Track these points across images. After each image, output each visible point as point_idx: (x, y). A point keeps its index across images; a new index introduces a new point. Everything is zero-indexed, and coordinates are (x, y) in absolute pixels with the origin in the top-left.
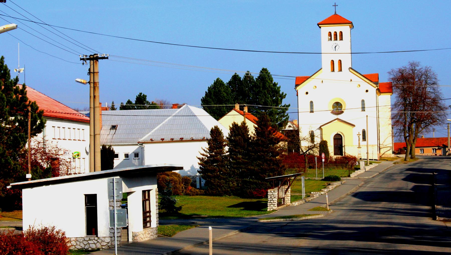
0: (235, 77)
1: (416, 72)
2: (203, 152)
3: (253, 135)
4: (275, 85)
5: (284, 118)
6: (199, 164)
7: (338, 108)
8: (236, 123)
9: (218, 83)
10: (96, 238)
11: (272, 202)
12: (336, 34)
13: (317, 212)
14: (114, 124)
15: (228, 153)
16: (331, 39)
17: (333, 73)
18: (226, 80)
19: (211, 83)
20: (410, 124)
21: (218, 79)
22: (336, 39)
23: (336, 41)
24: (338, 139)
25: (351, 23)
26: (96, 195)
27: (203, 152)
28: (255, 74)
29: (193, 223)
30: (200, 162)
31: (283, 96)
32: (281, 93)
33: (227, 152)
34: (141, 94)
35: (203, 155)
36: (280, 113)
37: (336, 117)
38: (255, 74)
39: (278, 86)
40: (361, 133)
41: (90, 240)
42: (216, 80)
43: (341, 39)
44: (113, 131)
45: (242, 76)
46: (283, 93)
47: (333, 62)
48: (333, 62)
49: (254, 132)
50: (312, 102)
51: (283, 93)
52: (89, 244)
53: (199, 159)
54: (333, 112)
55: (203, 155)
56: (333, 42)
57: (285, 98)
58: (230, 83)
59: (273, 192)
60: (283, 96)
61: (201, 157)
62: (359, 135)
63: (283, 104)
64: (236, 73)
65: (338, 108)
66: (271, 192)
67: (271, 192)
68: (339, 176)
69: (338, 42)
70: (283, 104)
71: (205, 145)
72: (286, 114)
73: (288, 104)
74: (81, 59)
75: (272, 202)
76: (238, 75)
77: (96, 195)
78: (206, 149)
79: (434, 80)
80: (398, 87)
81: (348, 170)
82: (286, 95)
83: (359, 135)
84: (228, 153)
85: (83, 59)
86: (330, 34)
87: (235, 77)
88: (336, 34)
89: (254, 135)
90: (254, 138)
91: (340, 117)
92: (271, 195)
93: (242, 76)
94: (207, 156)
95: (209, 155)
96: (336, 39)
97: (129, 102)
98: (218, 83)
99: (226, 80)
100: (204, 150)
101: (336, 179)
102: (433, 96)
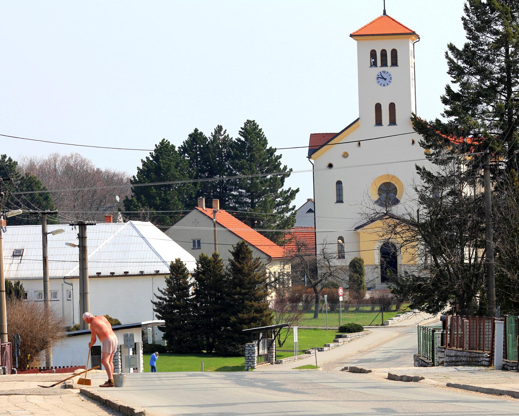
0: (196, 137)
2: (160, 295)
5: (290, 213)
6: (155, 310)
8: (205, 255)
9: (164, 149)
11: (250, 358)
12: (384, 53)
14: (18, 247)
15: (194, 296)
17: (379, 127)
18: (178, 141)
21: (162, 143)
22: (384, 64)
23: (384, 69)
25: (413, 33)
27: (160, 295)
28: (234, 133)
30: (155, 308)
31: (286, 173)
32: (282, 167)
34: (4, 157)
35: (161, 298)
36: (279, 204)
38: (234, 133)
42: (158, 144)
43: (395, 63)
44: (17, 260)
45: (208, 133)
46: (285, 168)
47: (378, 107)
48: (378, 107)
50: (339, 183)
51: (285, 168)
55: (161, 298)
56: (379, 69)
57: (288, 175)
58: (185, 149)
59: (251, 346)
60: (286, 173)
61: (157, 300)
63: (285, 188)
64: (196, 130)
66: (249, 346)
67: (249, 346)
68: (361, 324)
69: (390, 69)
70: (285, 188)
71: (164, 286)
72: (291, 206)
73: (294, 189)
75: (250, 358)
76: (201, 133)
78: (163, 291)
81: (381, 313)
82: (291, 170)
84: (194, 296)
86: (373, 54)
87: (196, 137)
88: (384, 53)
92: (249, 350)
94: (165, 299)
95: (168, 299)
98: (164, 149)
99: (178, 141)
100: (161, 291)
101: (357, 329)
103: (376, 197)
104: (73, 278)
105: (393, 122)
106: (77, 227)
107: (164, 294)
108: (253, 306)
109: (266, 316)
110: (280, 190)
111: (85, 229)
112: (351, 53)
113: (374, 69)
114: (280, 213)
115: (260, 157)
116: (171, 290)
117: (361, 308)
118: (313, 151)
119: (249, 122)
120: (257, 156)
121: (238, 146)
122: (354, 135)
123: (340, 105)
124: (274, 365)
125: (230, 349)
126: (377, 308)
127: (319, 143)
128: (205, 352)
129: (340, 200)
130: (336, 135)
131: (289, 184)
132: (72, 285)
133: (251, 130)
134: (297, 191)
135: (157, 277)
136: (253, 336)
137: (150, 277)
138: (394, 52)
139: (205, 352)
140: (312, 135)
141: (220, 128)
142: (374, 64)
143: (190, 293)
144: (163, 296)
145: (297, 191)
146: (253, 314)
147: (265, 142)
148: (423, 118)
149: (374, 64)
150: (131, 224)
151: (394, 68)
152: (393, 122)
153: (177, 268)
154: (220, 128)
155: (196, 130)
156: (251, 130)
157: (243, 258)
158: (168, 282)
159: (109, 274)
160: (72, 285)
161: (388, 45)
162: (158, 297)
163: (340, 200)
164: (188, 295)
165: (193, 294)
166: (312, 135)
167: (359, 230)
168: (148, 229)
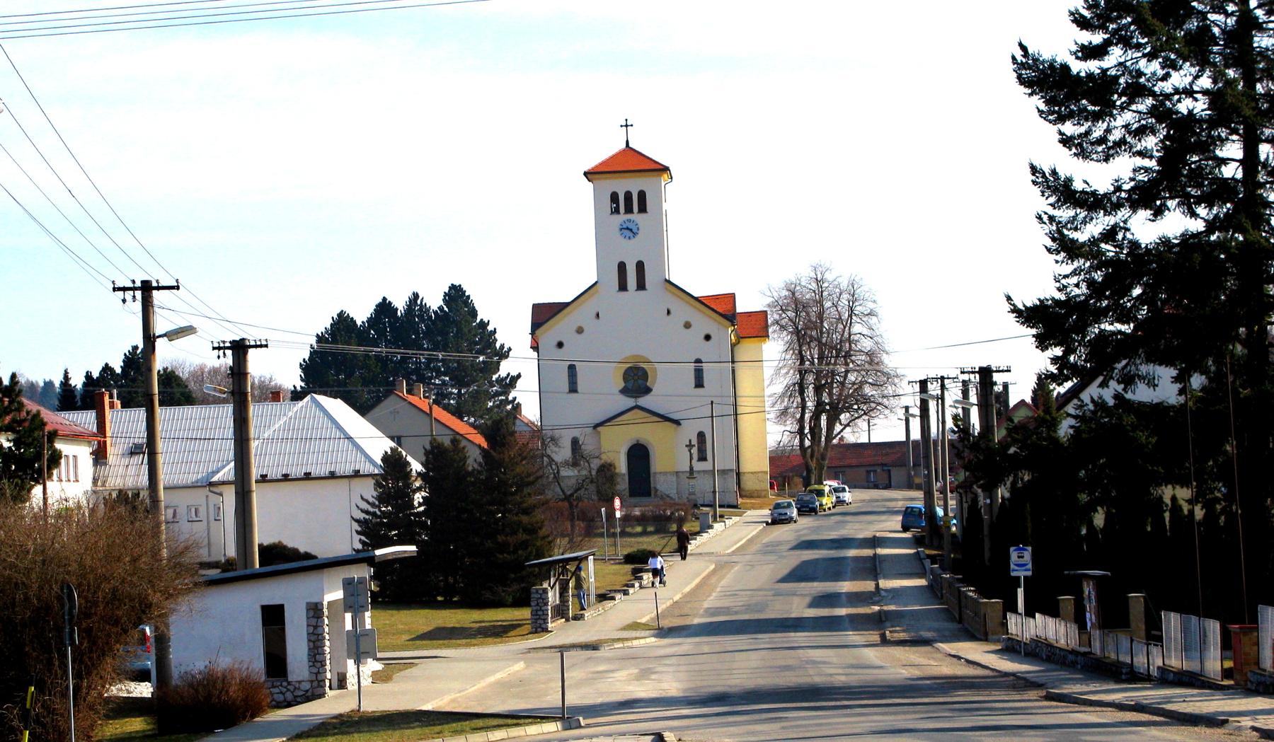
0: (384, 308)
1: (826, 285)
2: (365, 506)
3: (476, 466)
4: (484, 325)
6: (358, 533)
7: (637, 381)
9: (343, 324)
10: (285, 684)
12: (628, 196)
13: (638, 634)
16: (617, 211)
18: (361, 314)
19: (323, 323)
20: (816, 417)
21: (341, 314)
22: (629, 210)
23: (629, 216)
24: (639, 455)
26: (282, 607)
27: (365, 506)
28: (434, 300)
29: (713, 615)
31: (504, 354)
32: (498, 345)
33: (420, 505)
35: (367, 512)
36: (497, 394)
37: (630, 402)
38: (434, 300)
39: (490, 328)
40: (694, 442)
41: (273, 687)
43: (643, 209)
47: (622, 267)
48: (622, 267)
49: (480, 459)
51: (502, 346)
52: (272, 694)
53: (357, 521)
54: (624, 391)
55: (367, 512)
56: (622, 217)
57: (507, 357)
60: (504, 354)
61: (361, 516)
62: (690, 446)
63: (503, 372)
64: (384, 299)
65: (637, 381)
69: (636, 217)
70: (503, 372)
72: (510, 398)
73: (514, 373)
74: (214, 348)
77: (282, 607)
78: (371, 500)
79: (871, 305)
80: (783, 328)
82: (510, 349)
83: (690, 446)
84: (422, 509)
85: (219, 348)
86: (614, 198)
87: (384, 308)
88: (628, 196)
89: (480, 464)
90: (479, 472)
91: (644, 401)
93: (400, 303)
96: (629, 210)
97: (107, 369)
98: (343, 324)
99: (361, 314)
102: (866, 344)
103: (622, 385)
104: (223, 483)
105: (641, 286)
106: (229, 352)
107: (373, 505)
108: (520, 522)
109: (543, 538)
110: (494, 377)
111: (245, 353)
112: (583, 200)
113: (615, 216)
114: (498, 406)
115: (470, 331)
116: (383, 499)
117: (629, 530)
118: (536, 326)
119: (453, 287)
120: (466, 330)
121: (441, 316)
122: (589, 307)
123: (571, 268)
124: (572, 622)
125: (488, 595)
126: (650, 529)
127: (544, 315)
128: (440, 598)
129: (573, 389)
130: (566, 305)
131: (506, 368)
132: (221, 495)
133: (456, 296)
134: (519, 376)
135: (356, 481)
136: (544, 572)
137: (346, 481)
138: (642, 195)
139: (440, 598)
140: (534, 306)
141: (416, 296)
142: (617, 211)
143: (416, 503)
144: (371, 510)
145: (519, 376)
146: (522, 536)
147: (474, 313)
148: (1046, 56)
149: (616, 211)
150: (313, 398)
151: (643, 215)
152: (641, 286)
153: (394, 463)
154: (416, 296)
155: (384, 299)
156: (456, 296)
157: (503, 445)
158: (378, 485)
159: (279, 477)
160: (221, 495)
161: (633, 185)
162: (363, 511)
163: (573, 389)
164: (413, 507)
165: (420, 505)
166: (534, 306)
167: (599, 429)
168: (338, 408)
